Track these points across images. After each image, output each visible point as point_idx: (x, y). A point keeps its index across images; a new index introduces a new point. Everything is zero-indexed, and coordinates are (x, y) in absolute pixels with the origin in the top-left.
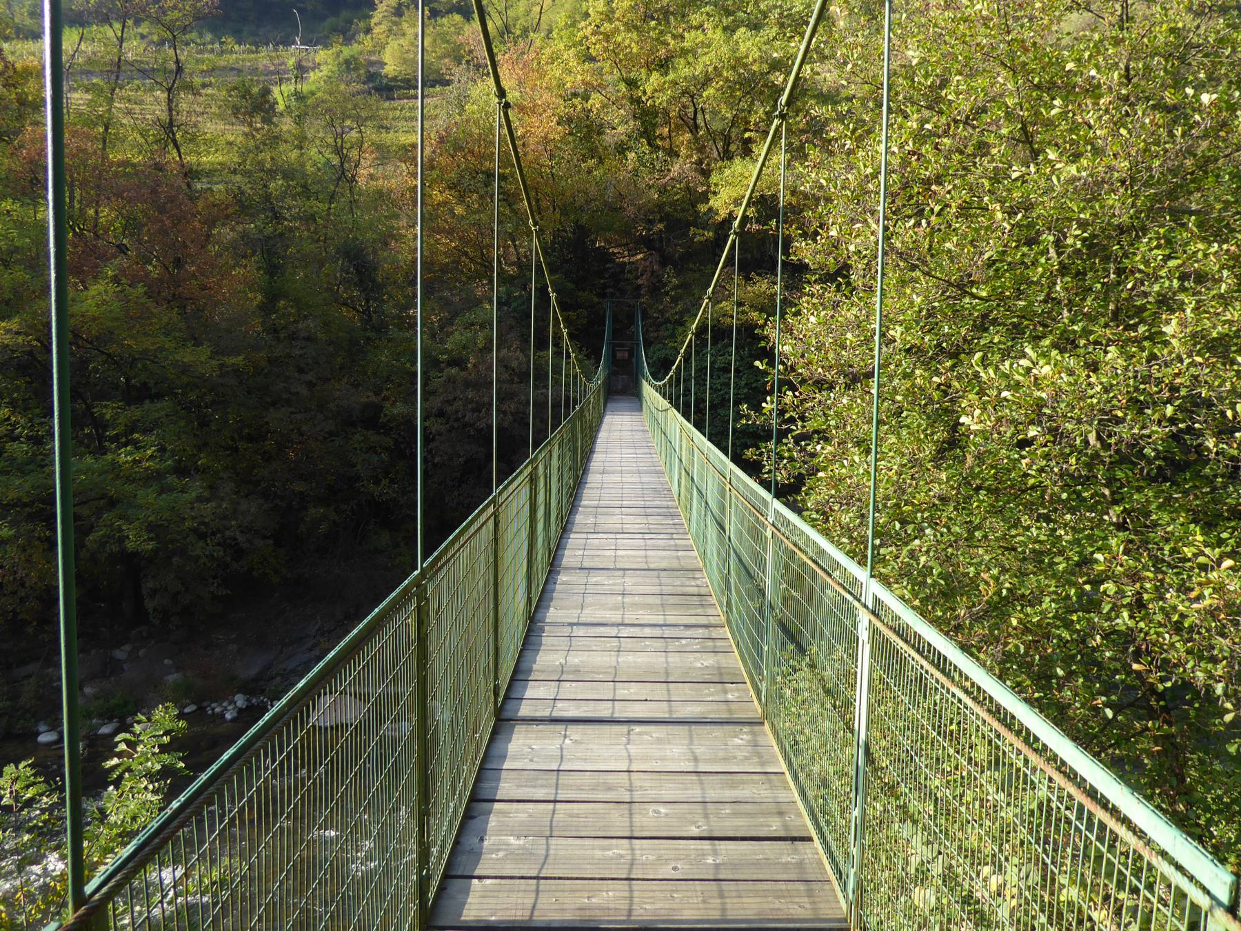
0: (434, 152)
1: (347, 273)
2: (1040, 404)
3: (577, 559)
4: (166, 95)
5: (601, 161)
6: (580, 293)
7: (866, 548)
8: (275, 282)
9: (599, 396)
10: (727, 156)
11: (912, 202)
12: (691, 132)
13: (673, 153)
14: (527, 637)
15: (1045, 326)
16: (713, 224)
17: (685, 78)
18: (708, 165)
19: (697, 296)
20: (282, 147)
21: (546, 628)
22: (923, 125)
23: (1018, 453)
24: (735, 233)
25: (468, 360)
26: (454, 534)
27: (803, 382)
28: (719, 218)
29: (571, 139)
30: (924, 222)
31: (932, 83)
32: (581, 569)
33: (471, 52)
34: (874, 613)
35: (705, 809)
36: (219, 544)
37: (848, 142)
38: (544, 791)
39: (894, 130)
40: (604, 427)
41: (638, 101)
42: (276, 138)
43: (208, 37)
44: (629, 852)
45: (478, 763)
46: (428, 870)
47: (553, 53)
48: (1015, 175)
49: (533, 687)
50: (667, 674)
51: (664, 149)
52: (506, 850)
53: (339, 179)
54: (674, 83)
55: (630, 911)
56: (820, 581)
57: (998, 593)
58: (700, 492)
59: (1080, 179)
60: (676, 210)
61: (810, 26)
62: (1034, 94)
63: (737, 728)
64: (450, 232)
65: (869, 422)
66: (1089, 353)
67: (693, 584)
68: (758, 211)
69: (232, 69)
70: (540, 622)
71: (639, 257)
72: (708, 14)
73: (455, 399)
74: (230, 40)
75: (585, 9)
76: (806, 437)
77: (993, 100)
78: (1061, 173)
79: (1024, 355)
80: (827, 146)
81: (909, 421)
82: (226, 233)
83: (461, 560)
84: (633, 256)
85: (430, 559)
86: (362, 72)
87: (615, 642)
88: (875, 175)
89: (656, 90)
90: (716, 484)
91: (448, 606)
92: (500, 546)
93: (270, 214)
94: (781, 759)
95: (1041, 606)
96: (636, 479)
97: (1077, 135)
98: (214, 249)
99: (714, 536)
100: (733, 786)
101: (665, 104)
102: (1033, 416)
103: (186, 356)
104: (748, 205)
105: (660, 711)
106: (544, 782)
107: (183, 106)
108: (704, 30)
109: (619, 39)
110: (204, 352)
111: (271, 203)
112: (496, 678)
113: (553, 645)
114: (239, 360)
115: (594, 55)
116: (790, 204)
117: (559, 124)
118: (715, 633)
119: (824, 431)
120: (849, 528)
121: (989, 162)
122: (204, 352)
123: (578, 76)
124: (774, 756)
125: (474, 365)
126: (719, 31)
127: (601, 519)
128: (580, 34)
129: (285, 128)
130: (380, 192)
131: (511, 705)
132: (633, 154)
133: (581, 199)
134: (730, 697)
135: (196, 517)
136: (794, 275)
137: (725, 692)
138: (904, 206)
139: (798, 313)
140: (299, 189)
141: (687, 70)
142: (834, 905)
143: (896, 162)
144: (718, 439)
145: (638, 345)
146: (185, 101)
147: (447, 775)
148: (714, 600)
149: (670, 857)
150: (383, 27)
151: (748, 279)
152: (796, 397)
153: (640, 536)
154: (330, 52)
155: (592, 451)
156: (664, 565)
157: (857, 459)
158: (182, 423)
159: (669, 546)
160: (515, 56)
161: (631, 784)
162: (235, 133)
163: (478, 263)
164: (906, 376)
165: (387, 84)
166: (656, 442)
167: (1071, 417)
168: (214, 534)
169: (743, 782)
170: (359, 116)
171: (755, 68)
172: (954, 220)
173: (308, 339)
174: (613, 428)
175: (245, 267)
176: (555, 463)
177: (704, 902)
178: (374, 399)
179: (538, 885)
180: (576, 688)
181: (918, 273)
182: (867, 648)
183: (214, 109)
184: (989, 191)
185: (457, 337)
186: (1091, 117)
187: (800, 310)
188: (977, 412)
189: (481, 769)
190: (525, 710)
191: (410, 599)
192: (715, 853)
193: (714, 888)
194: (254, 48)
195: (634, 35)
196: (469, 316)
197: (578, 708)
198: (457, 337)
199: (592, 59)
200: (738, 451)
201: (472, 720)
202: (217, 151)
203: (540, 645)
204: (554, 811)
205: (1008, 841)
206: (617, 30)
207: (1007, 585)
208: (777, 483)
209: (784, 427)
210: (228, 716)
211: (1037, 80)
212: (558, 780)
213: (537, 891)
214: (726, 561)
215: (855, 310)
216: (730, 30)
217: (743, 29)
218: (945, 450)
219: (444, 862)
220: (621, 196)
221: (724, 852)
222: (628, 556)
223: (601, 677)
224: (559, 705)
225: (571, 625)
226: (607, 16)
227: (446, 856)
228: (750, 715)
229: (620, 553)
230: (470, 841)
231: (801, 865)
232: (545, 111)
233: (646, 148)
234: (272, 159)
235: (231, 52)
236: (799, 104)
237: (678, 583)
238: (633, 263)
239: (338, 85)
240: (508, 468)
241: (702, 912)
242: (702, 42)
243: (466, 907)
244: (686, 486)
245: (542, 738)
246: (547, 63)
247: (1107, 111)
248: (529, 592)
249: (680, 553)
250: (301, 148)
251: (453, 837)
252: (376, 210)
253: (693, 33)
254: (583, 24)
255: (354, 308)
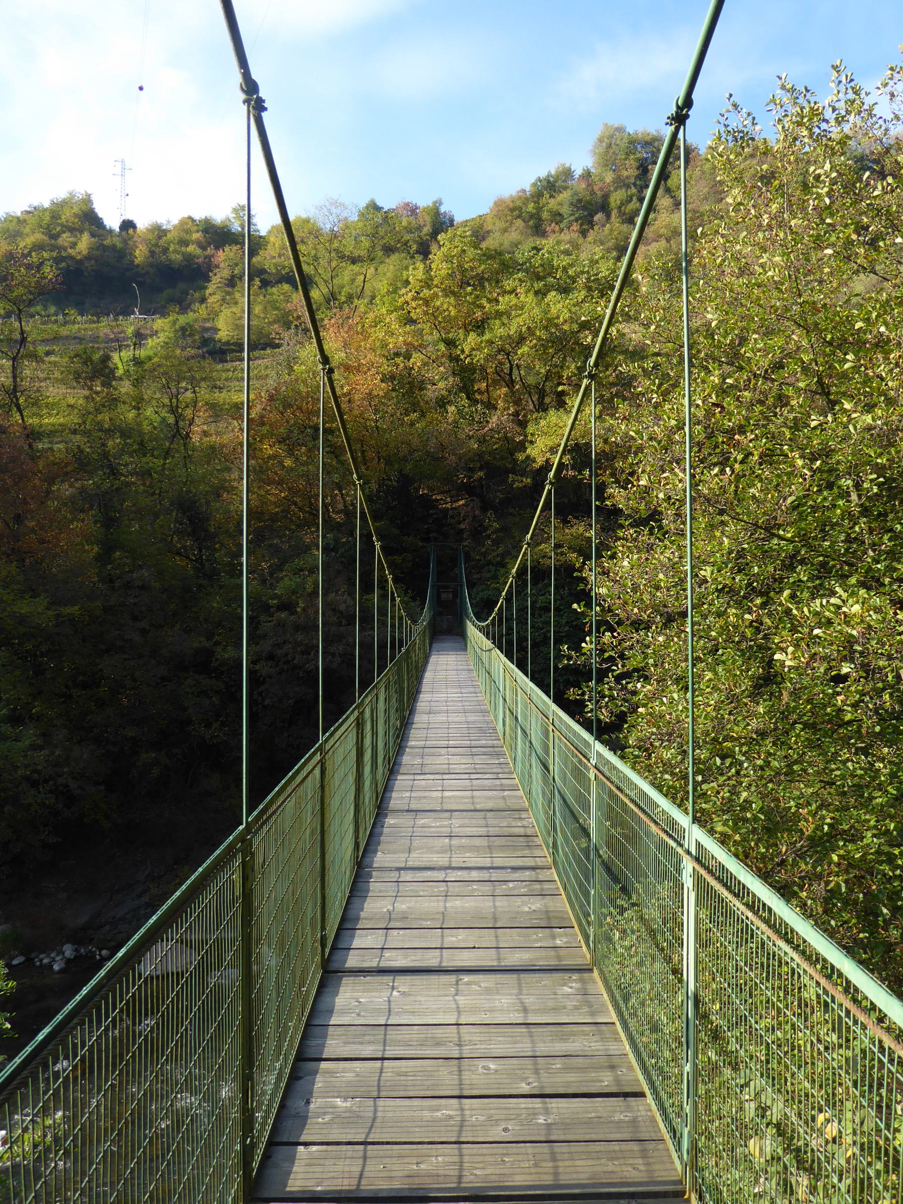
0: (264, 409)
1: (181, 524)
2: (850, 641)
3: (405, 801)
4: (11, 363)
5: (423, 415)
6: (405, 538)
7: (687, 785)
8: (112, 534)
9: (424, 637)
10: (542, 408)
11: (718, 450)
12: (508, 386)
13: (491, 406)
14: (355, 882)
15: (851, 565)
16: (531, 471)
17: (501, 337)
18: (525, 416)
19: (517, 539)
20: (122, 408)
21: (374, 873)
22: (724, 379)
23: (833, 688)
24: (551, 483)
25: (298, 604)
26: (280, 785)
27: (620, 623)
28: (536, 466)
29: (394, 394)
30: (728, 469)
31: (731, 341)
32: (408, 811)
33: (299, 317)
34: (697, 860)
35: (535, 1064)
36: (51, 792)
37: (655, 396)
38: (371, 1048)
39: (697, 384)
40: (430, 667)
41: (457, 359)
42: (115, 399)
43: (52, 309)
44: (459, 1113)
45: (304, 1019)
46: (252, 1138)
47: (376, 317)
48: (813, 424)
49: (361, 936)
50: (495, 919)
51: (482, 403)
52: (332, 1113)
53: (174, 436)
54: (490, 342)
55: (460, 1177)
56: (643, 826)
57: (819, 828)
58: (524, 732)
59: (875, 428)
60: (495, 458)
61: (616, 292)
62: (828, 350)
63: (566, 976)
64: (280, 483)
65: (686, 660)
66: (894, 591)
67: (520, 824)
68: (573, 458)
69: (75, 338)
70: (367, 867)
71: (461, 503)
72: (520, 280)
73: (285, 642)
74: (72, 312)
75: (405, 278)
76: (627, 675)
77: (789, 355)
78: (857, 422)
79: (833, 593)
80: (634, 399)
81: (724, 658)
82: (66, 490)
83: (288, 810)
84: (455, 502)
85: (255, 813)
86: (197, 337)
87: (442, 887)
88: (680, 427)
89: (473, 349)
90: (539, 724)
91: (274, 859)
92: (327, 793)
93: (108, 471)
94: (611, 1008)
95: (862, 841)
96: (461, 718)
97: (870, 387)
98: (53, 504)
99: (539, 776)
100: (564, 1038)
101: (482, 362)
102: (845, 653)
103: (24, 608)
104: (563, 453)
105: (487, 959)
106: (371, 1038)
107: (27, 372)
108: (517, 295)
109: (438, 303)
110: (41, 602)
111: (109, 461)
112: (323, 928)
113: (380, 891)
114: (74, 610)
115: (414, 318)
116: (604, 451)
117: (382, 381)
118: (543, 875)
119: (643, 669)
120: (670, 764)
121: (788, 412)
122: (41, 602)
123: (400, 337)
124: (604, 1005)
125: (304, 609)
126: (531, 295)
127: (428, 760)
128: (401, 300)
129: (123, 390)
130: (213, 448)
131: (338, 955)
132: (453, 408)
133: (404, 449)
134: (558, 942)
135: (29, 765)
136: (609, 517)
137: (554, 937)
138: (710, 454)
139: (613, 557)
140: (135, 447)
141: (502, 330)
142: (668, 1166)
143: (700, 414)
144: (540, 681)
145: (462, 586)
146: (28, 369)
147: (272, 1036)
148: (540, 841)
149: (500, 1117)
150: (217, 297)
151: (565, 522)
152: (614, 637)
153: (466, 776)
154: (166, 321)
155: (418, 692)
156: (490, 805)
157: (675, 696)
158: (18, 672)
159: (496, 785)
160: (340, 321)
161: (460, 1038)
162: (77, 396)
163: (307, 512)
164: (720, 615)
165: (220, 348)
166: (481, 681)
167: (882, 654)
168: (46, 781)
169: (573, 1034)
170: (193, 378)
171: (566, 327)
172: (757, 467)
173: (142, 588)
174: (439, 668)
175: (83, 521)
176: (381, 705)
177: (536, 1165)
178: (207, 644)
179: (365, 1151)
180: (404, 935)
181: (726, 518)
182: (693, 896)
183: (57, 375)
184: (790, 439)
185: (286, 583)
186: (882, 370)
187: (615, 553)
188: (791, 649)
189: (308, 1025)
190: (352, 961)
191: (234, 856)
192: (547, 1112)
193: (546, 1150)
194: (95, 318)
195: (452, 300)
196: (298, 562)
197: (406, 957)
198: (286, 583)
199: (413, 322)
200: (561, 688)
201: (299, 973)
202: (57, 414)
203: (368, 891)
204: (382, 1069)
205: (840, 1084)
206: (435, 295)
207: (828, 821)
208: (599, 721)
209: (604, 666)
210: (56, 967)
211: (829, 336)
212: (385, 1035)
213: (365, 1158)
214: (550, 802)
215: (668, 554)
216: (541, 294)
217: (553, 293)
218: (761, 686)
219: (268, 1128)
220: (442, 447)
221: (555, 1110)
222: (454, 797)
223: (428, 924)
224: (387, 954)
225: (399, 869)
226: (426, 283)
227: (271, 1122)
228: (579, 961)
229: (447, 794)
230: (296, 1104)
231: (634, 1122)
232: (369, 369)
233: (465, 402)
234: (111, 419)
235: (74, 323)
236: (608, 359)
237: (505, 824)
238: (455, 508)
239: (173, 351)
240: (334, 715)
241: (534, 1177)
242: (516, 305)
243: (292, 1176)
244: (510, 726)
245: (369, 991)
246: (371, 326)
247: (897, 365)
248: (357, 838)
249: (506, 793)
250: (139, 409)
251: (278, 1100)
252: (208, 464)
253: (507, 297)
254: (404, 291)
255: (188, 557)
